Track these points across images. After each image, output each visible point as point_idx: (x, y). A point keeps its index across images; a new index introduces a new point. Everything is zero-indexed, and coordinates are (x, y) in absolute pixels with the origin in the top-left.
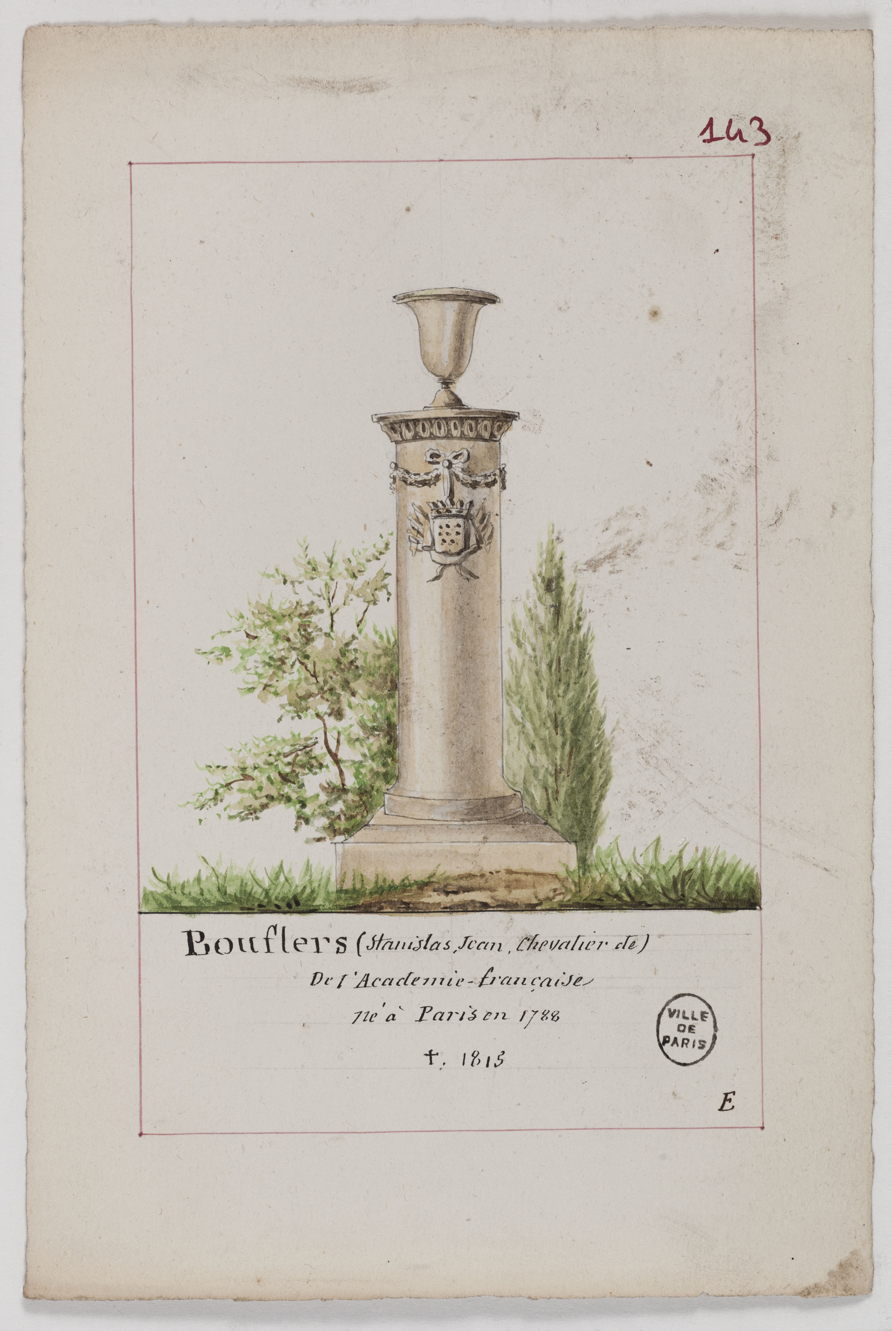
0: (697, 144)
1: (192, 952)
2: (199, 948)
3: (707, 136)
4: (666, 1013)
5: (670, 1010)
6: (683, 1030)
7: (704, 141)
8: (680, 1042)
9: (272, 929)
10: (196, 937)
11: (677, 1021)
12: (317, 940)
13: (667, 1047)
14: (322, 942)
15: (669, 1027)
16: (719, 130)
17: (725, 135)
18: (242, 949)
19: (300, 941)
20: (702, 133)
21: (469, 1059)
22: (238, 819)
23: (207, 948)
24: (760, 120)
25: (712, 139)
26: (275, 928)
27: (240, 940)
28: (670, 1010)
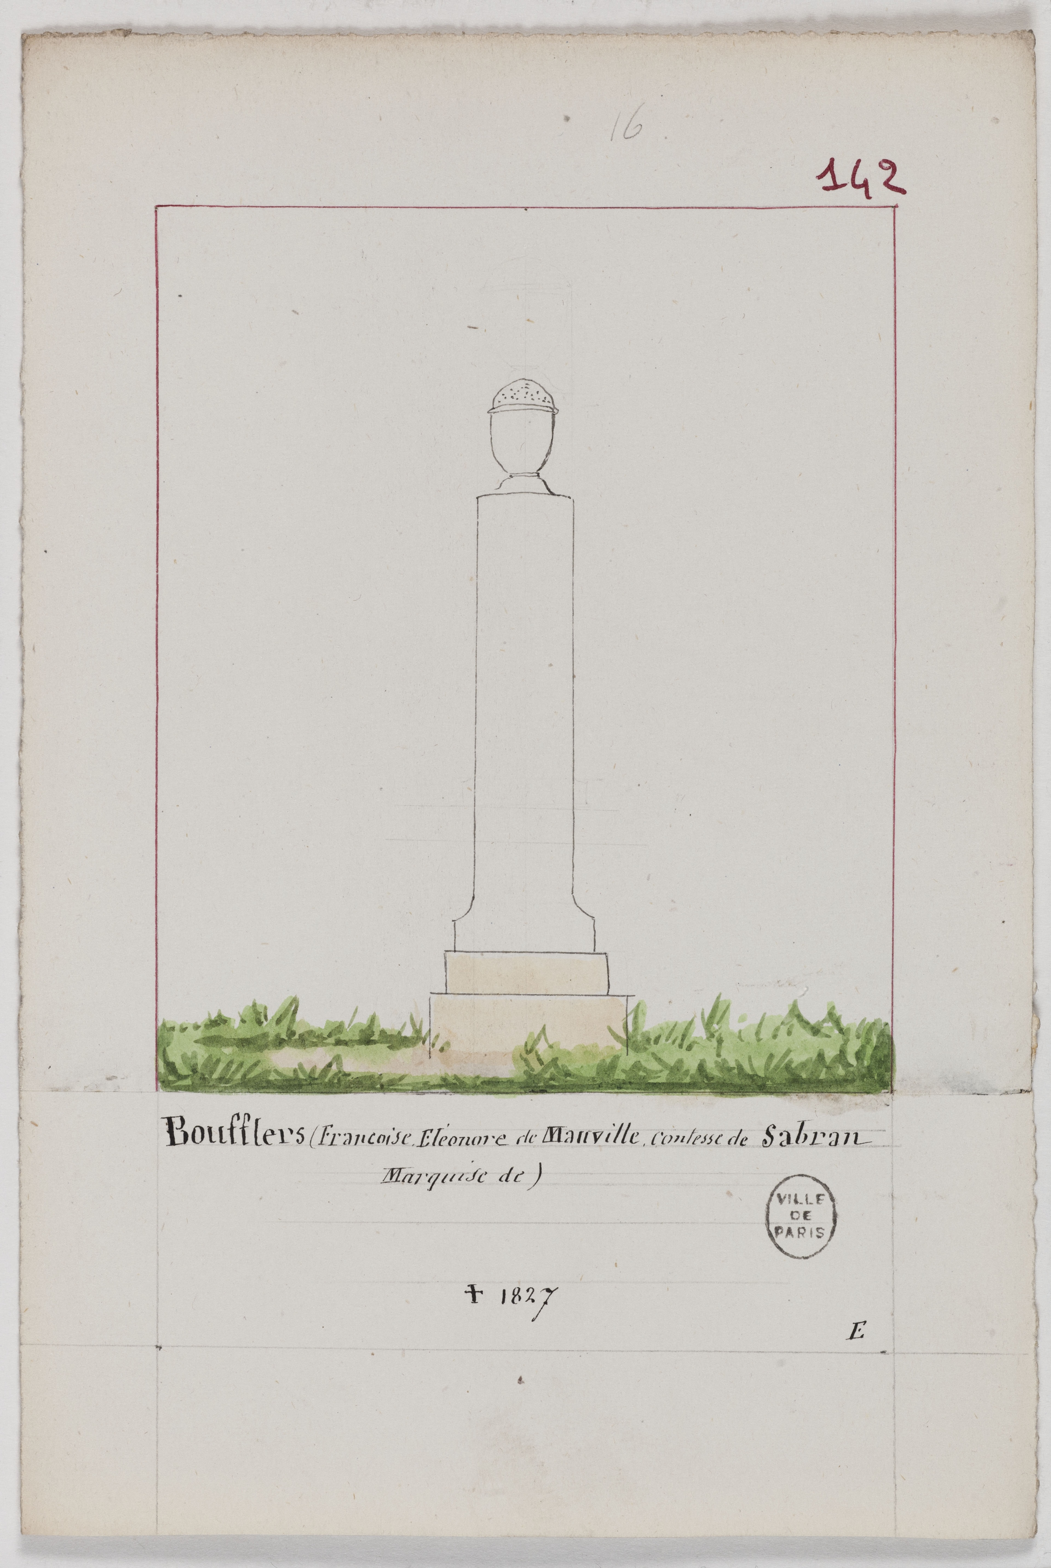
0: (815, 191)
1: (173, 1143)
2: (179, 1136)
3: (828, 181)
4: (775, 1198)
5: (779, 1195)
6: (794, 1222)
7: (826, 188)
8: (795, 1232)
9: (236, 1117)
10: (177, 1123)
11: (788, 1206)
12: (282, 1131)
13: (781, 1239)
14: (287, 1133)
15: (780, 1215)
16: (843, 175)
17: (848, 180)
18: (211, 1141)
19: (269, 1133)
20: (820, 177)
21: (509, 1297)
22: (526, 1068)
23: (186, 1135)
24: (893, 167)
25: (836, 186)
26: (238, 1115)
27: (220, 1129)
28: (779, 1195)
